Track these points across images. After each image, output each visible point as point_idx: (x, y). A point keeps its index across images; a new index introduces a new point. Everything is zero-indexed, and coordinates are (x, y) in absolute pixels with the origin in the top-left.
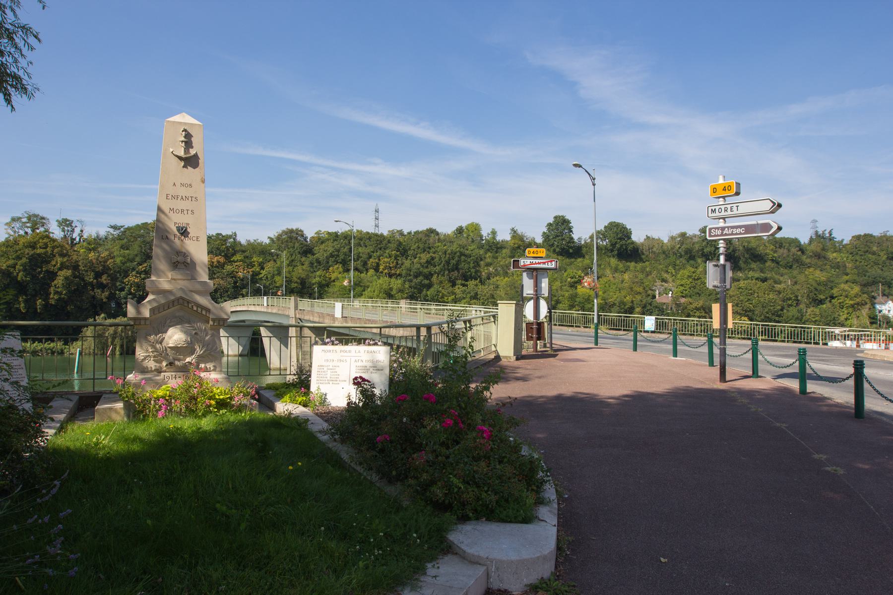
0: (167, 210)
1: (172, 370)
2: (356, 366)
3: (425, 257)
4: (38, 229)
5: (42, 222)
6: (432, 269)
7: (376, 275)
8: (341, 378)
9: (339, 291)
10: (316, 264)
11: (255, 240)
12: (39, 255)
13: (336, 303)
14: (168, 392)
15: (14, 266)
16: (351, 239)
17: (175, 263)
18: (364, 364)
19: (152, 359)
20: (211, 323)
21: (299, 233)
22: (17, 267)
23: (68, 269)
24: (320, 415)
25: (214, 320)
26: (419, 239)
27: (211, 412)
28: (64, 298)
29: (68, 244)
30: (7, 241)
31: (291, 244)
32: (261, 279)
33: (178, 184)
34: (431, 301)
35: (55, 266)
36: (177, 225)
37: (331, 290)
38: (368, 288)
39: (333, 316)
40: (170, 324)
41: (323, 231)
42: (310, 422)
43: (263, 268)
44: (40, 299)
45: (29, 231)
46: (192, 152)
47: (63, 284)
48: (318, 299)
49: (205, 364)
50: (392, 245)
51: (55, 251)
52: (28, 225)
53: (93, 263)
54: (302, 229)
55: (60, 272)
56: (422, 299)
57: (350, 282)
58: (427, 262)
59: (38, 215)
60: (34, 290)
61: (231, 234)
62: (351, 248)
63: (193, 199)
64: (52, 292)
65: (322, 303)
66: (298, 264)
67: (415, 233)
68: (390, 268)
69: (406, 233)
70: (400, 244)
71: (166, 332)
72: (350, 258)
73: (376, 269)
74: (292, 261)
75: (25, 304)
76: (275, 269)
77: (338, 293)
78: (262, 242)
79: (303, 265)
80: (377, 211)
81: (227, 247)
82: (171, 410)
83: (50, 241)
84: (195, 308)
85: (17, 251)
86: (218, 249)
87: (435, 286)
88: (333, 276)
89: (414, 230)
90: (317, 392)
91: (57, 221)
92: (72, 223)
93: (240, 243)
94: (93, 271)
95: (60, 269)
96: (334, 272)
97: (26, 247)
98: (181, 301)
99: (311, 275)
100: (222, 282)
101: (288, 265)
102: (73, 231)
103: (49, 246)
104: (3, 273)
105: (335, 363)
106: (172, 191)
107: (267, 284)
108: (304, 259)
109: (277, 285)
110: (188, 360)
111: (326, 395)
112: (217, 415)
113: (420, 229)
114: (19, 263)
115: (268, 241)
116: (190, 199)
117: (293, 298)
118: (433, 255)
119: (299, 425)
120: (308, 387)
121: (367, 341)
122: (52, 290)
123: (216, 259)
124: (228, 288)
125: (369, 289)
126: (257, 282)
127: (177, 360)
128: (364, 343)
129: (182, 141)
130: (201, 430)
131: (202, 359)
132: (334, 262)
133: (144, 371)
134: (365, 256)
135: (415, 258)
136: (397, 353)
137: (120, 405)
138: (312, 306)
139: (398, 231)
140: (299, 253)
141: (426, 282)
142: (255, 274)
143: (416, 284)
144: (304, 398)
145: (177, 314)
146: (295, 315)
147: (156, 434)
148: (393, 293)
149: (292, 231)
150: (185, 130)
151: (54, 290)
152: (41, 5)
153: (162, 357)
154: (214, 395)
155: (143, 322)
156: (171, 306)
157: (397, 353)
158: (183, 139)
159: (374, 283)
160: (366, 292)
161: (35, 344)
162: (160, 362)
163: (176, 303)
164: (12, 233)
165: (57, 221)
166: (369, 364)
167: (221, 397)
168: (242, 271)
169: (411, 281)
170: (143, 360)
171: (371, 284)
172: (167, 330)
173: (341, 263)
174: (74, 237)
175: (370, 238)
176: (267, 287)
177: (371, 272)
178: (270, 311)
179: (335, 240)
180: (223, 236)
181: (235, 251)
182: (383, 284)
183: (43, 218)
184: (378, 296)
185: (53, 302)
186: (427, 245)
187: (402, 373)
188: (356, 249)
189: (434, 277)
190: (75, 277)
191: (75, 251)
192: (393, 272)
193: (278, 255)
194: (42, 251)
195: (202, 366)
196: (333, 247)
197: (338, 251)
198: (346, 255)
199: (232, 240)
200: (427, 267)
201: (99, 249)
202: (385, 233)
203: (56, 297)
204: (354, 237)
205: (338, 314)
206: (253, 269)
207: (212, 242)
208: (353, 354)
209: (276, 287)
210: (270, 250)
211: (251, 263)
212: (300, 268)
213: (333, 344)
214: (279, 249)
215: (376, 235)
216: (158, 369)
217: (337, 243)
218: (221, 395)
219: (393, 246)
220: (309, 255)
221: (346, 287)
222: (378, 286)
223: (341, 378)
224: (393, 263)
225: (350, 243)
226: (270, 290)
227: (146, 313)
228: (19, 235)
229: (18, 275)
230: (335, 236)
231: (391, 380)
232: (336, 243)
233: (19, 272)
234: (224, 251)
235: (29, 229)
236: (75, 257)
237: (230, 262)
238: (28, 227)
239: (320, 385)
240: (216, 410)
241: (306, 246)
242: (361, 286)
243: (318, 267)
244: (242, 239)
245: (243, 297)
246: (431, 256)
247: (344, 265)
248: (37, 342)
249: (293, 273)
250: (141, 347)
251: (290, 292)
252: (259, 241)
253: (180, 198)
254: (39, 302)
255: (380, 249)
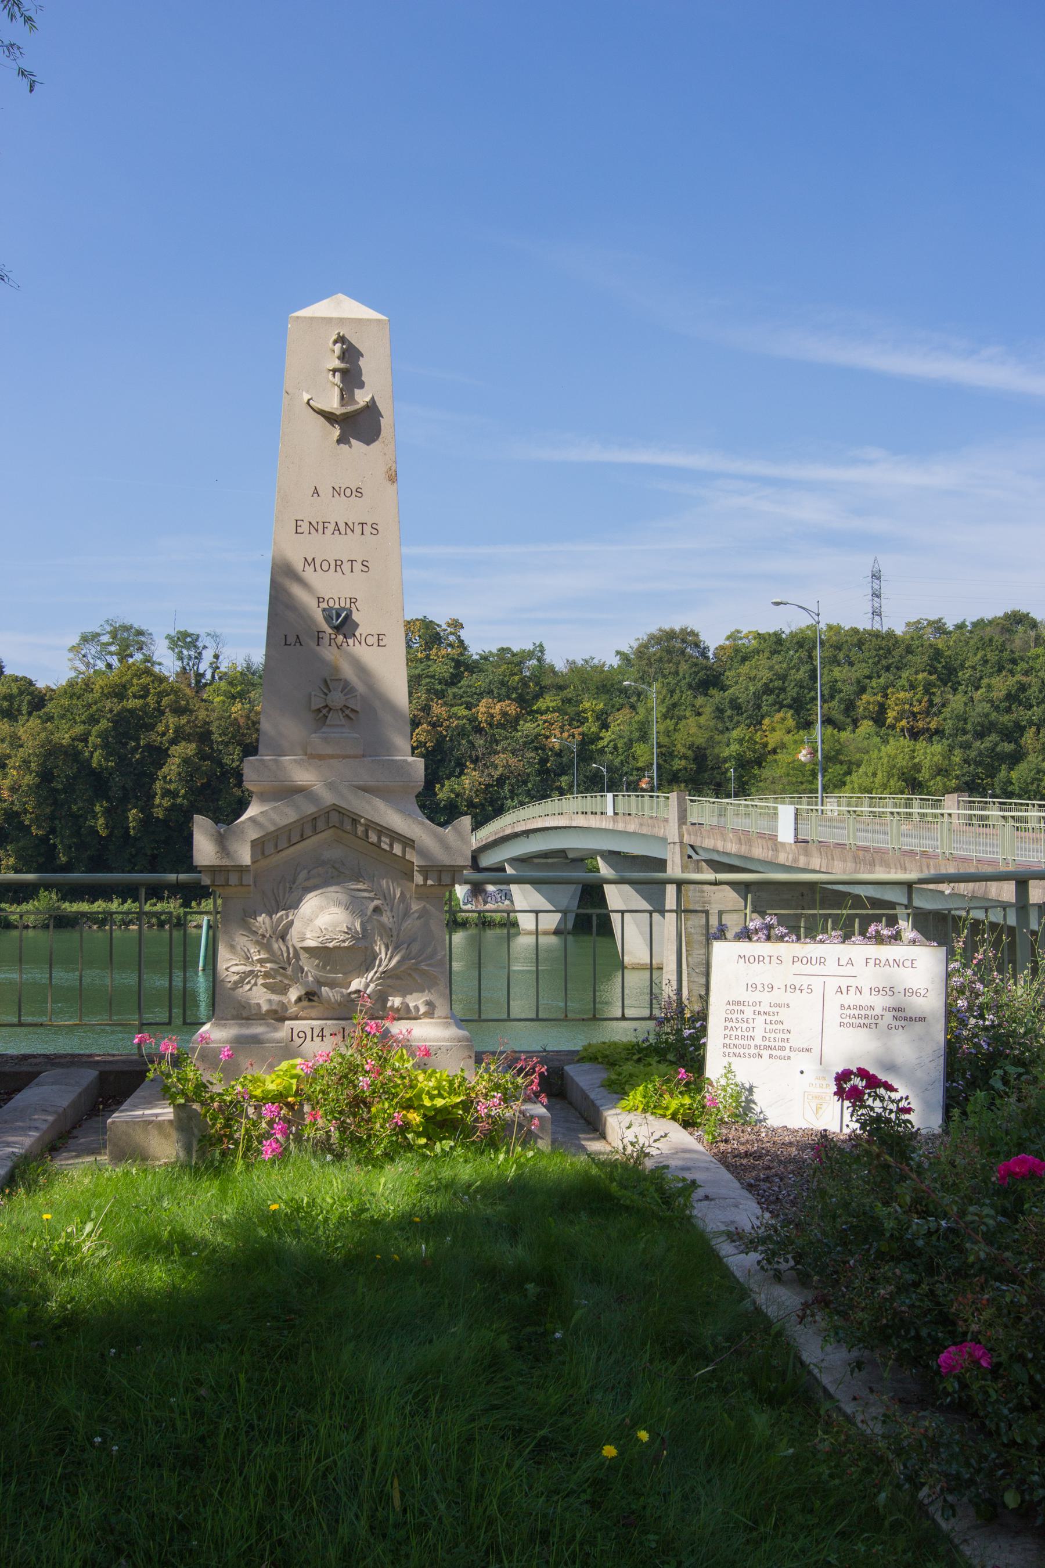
0: (298, 565)
1: (314, 1013)
2: (842, 1006)
3: (1001, 685)
4: (131, 656)
5: (138, 642)
6: (1020, 714)
7: (877, 734)
8: (795, 1041)
9: (788, 775)
10: (729, 712)
11: (586, 661)
12: (131, 711)
13: (781, 807)
14: (294, 1081)
15: (85, 740)
16: (815, 647)
17: (319, 710)
18: (866, 999)
19: (260, 981)
20: (419, 879)
21: (689, 638)
22: (91, 739)
23: (190, 742)
24: (728, 1161)
25: (425, 871)
26: (987, 639)
27: (410, 1147)
28: (181, 805)
29: (189, 685)
30: (71, 684)
31: (669, 667)
32: (602, 751)
33: (325, 491)
34: (1020, 797)
35: (164, 734)
36: (324, 605)
37: (766, 773)
38: (859, 766)
39: (773, 838)
40: (307, 884)
41: (745, 632)
42: (700, 1193)
43: (605, 726)
44: (134, 807)
45: (114, 661)
46: (362, 398)
47: (179, 774)
48: (736, 796)
49: (404, 996)
50: (918, 658)
51: (163, 703)
52: (113, 648)
53: (239, 726)
54: (696, 629)
55: (174, 747)
56: (998, 791)
57: (813, 753)
58: (1009, 697)
59: (131, 627)
60: (124, 788)
61: (532, 648)
62: (814, 670)
63: (367, 529)
64: (159, 791)
65: (747, 806)
66: (688, 714)
67: (975, 625)
68: (914, 715)
69: (950, 627)
70: (937, 654)
71: (295, 905)
72: (812, 694)
73: (879, 718)
74: (674, 705)
75: (105, 818)
76: (635, 726)
77: (785, 780)
78: (604, 665)
79: (699, 714)
80: (876, 576)
81: (522, 679)
82: (299, 1138)
83: (153, 682)
84: (373, 838)
85: (89, 706)
86: (503, 683)
87: (1031, 757)
88: (773, 740)
89: (971, 618)
90: (723, 1082)
91: (168, 637)
92: (197, 640)
93: (552, 668)
94: (239, 745)
95: (174, 742)
96: (774, 730)
97: (107, 696)
98: (334, 818)
99: (718, 738)
100: (513, 761)
101: (665, 717)
102: (199, 657)
103: (152, 691)
104: (66, 753)
105: (778, 996)
106: (310, 510)
107: (617, 762)
108: (700, 700)
109: (640, 764)
110: (356, 984)
111: (750, 1090)
112: (425, 1157)
113: (988, 616)
114: (95, 730)
115: (615, 662)
116: (358, 529)
117: (673, 796)
118: (1024, 679)
119: (667, 1198)
120: (696, 1064)
121: (872, 929)
122: (158, 786)
123: (498, 707)
124: (528, 775)
125: (861, 770)
126: (591, 759)
127: (325, 985)
128: (863, 933)
129: (334, 371)
130: (364, 1216)
131: (393, 981)
132: (773, 705)
133: (245, 1013)
134: (849, 689)
135: (977, 688)
136: (966, 966)
137: (165, 1112)
138: (722, 814)
139: (930, 623)
140: (690, 686)
141: (1008, 747)
142: (587, 741)
143: (980, 754)
144: (687, 1101)
145: (327, 855)
146: (681, 836)
147: (242, 1227)
148: (924, 775)
149: (671, 635)
150: (341, 339)
151: (162, 788)
152: (25, 83)
153: (286, 976)
154: (419, 1097)
155: (234, 879)
156: (308, 832)
157: (966, 966)
158: (337, 364)
159: (874, 754)
160: (854, 777)
161: (126, 905)
162: (284, 990)
163: (321, 824)
164: (83, 668)
165: (168, 637)
166: (879, 1002)
167: (439, 1102)
168: (557, 732)
169: (966, 746)
170: (239, 984)
171: (866, 757)
172: (300, 900)
173: (790, 707)
174: (201, 671)
175: (860, 644)
176: (617, 769)
177: (866, 726)
178: (620, 827)
179: (774, 652)
180: (514, 655)
181: (541, 688)
182: (895, 757)
183: (140, 633)
184: (885, 786)
185: (159, 813)
186: (1006, 655)
187: (986, 1029)
188: (826, 671)
189: (1026, 735)
190: (204, 757)
191: (203, 700)
192: (921, 724)
193: (639, 694)
194: (138, 703)
195: (396, 1001)
196: (771, 668)
197: (783, 678)
198: (801, 687)
199: (535, 662)
200: (1008, 710)
201: (252, 695)
202: (899, 630)
203: (166, 803)
204: (822, 643)
205: (786, 834)
206: (583, 729)
207: (490, 668)
208: (831, 967)
209: (638, 769)
210: (621, 682)
211: (578, 714)
212: (692, 721)
213: (768, 938)
214: (642, 678)
215: (877, 635)
216: (275, 1012)
217: (780, 658)
218: (440, 1095)
219: (919, 659)
220: (712, 691)
221: (804, 765)
222: (885, 760)
223: (795, 1041)
224: (920, 702)
225: (810, 657)
226: (622, 776)
227: (245, 856)
228: (95, 671)
229: (92, 757)
230: (775, 643)
231: (951, 1048)
232: (776, 658)
233: (95, 750)
234: (515, 689)
235: (115, 657)
236: (202, 714)
237: (531, 713)
238: (111, 654)
239: (732, 1059)
240: (423, 1141)
241: (706, 668)
242: (841, 763)
243: (736, 718)
244: (558, 658)
245: (562, 794)
246: (1018, 682)
247: (797, 712)
248: (129, 901)
249: (677, 736)
250: (232, 948)
251: (669, 780)
252: (596, 661)
253: (331, 527)
254: (133, 813)
255: (888, 669)
